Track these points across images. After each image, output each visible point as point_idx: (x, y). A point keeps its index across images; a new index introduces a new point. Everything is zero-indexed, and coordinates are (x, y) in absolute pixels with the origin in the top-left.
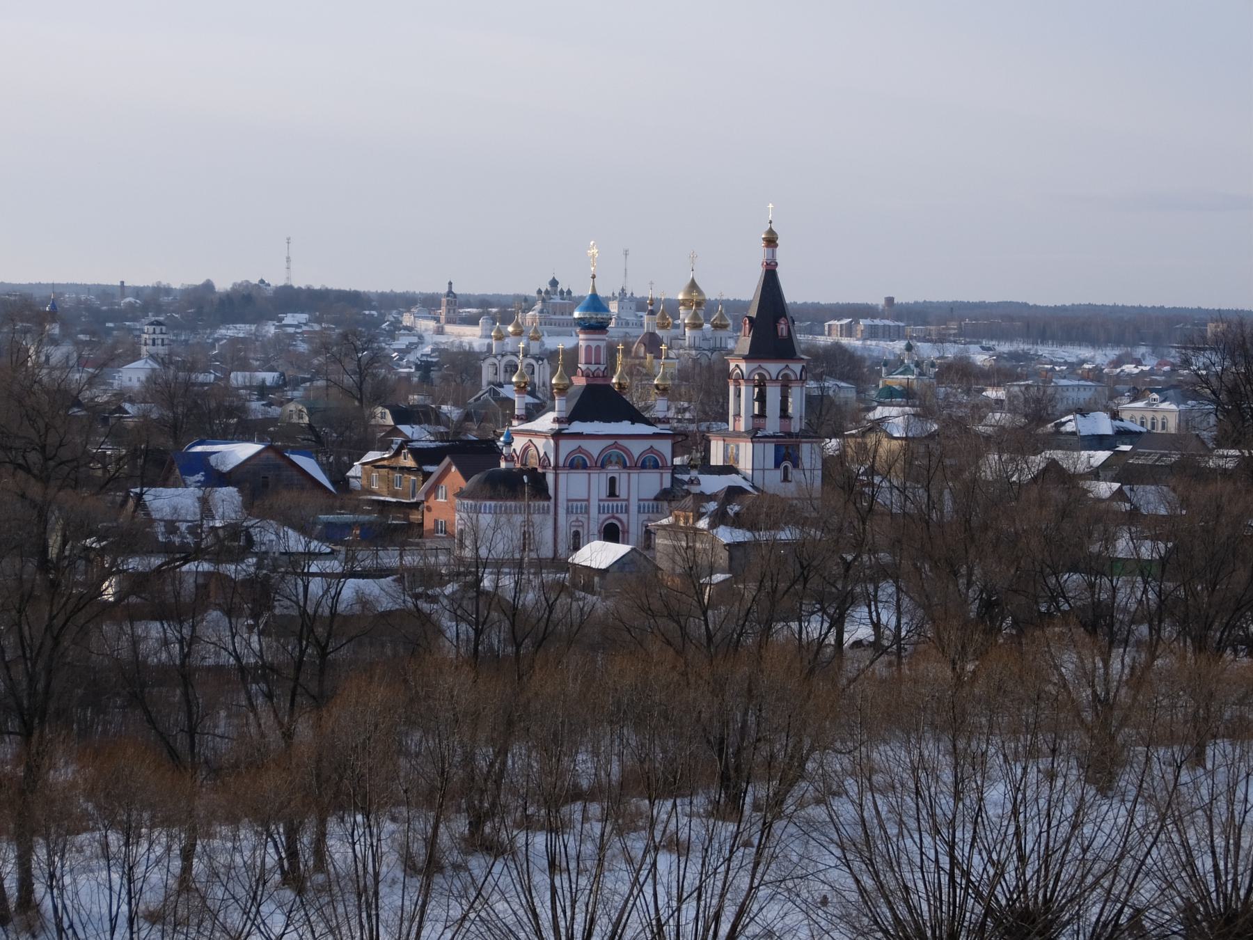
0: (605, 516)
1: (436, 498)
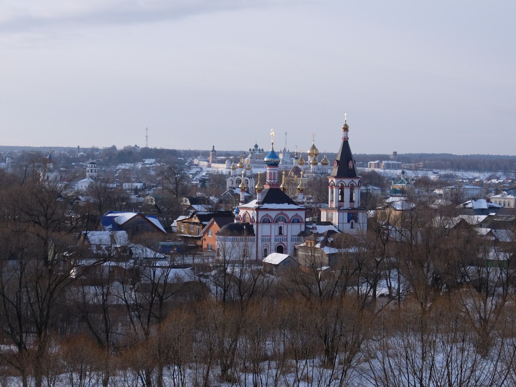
1: (208, 235)
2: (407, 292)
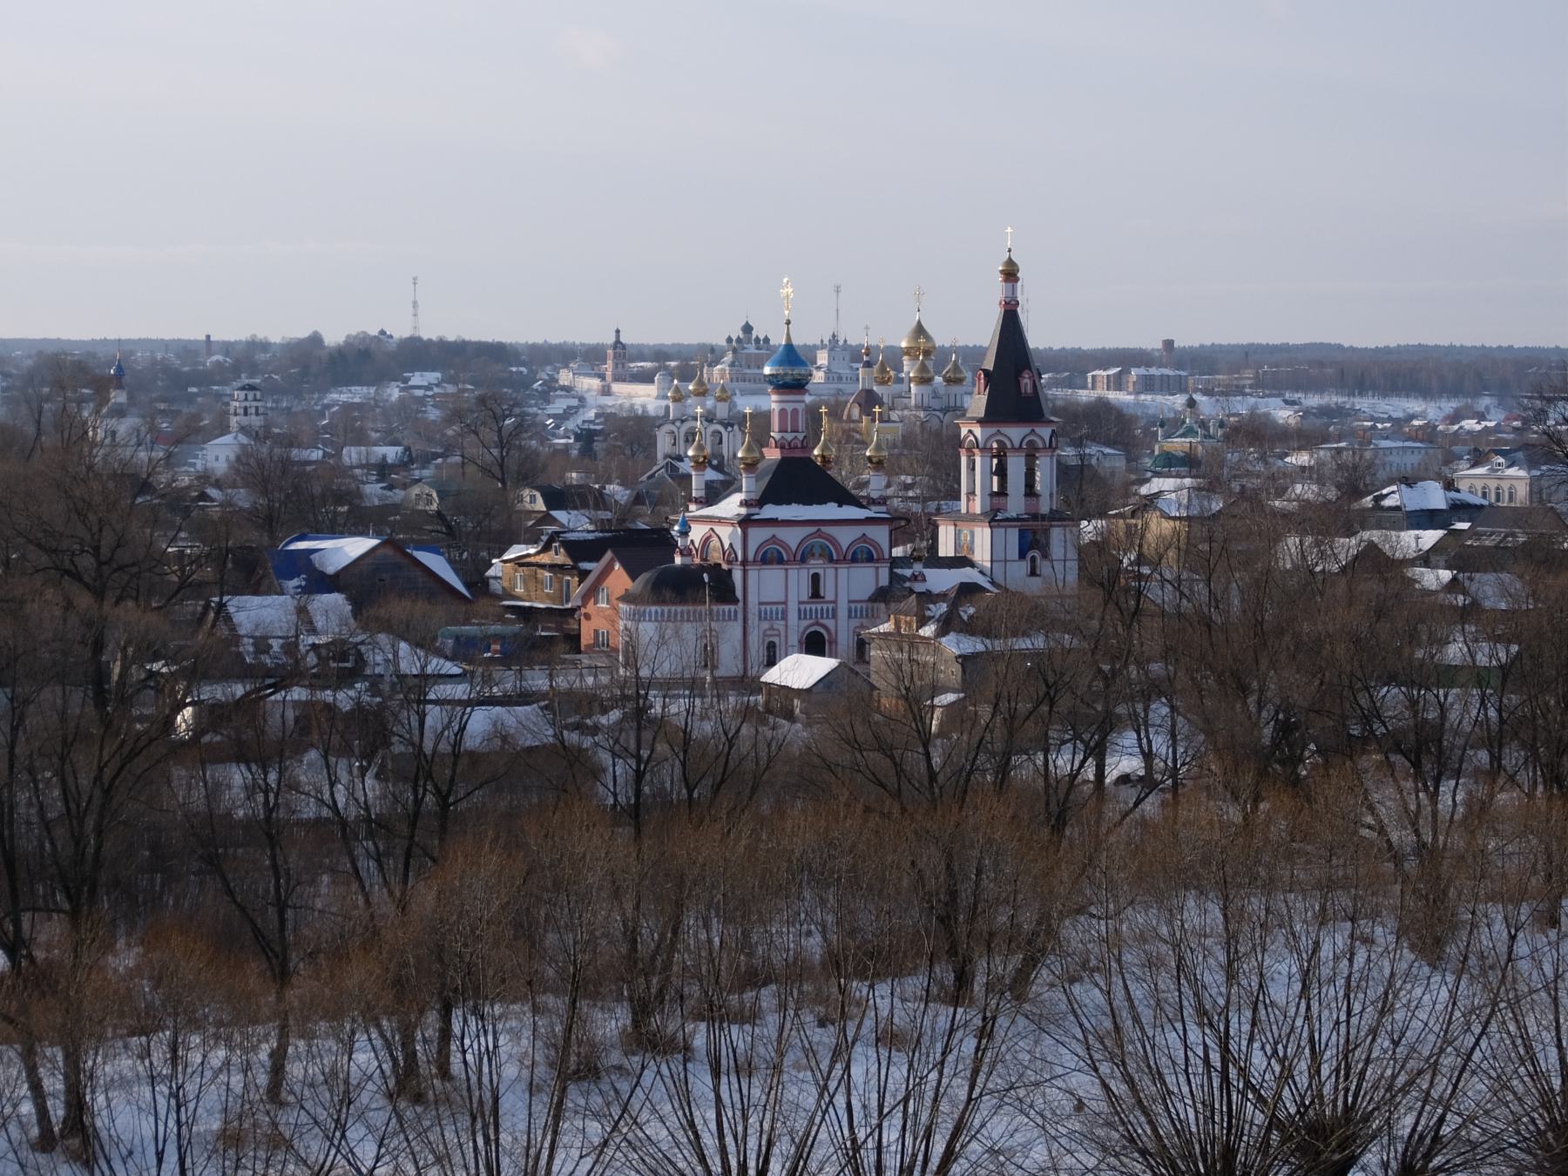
0: (805, 623)
2: (1201, 767)
